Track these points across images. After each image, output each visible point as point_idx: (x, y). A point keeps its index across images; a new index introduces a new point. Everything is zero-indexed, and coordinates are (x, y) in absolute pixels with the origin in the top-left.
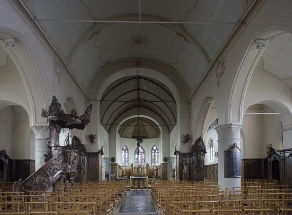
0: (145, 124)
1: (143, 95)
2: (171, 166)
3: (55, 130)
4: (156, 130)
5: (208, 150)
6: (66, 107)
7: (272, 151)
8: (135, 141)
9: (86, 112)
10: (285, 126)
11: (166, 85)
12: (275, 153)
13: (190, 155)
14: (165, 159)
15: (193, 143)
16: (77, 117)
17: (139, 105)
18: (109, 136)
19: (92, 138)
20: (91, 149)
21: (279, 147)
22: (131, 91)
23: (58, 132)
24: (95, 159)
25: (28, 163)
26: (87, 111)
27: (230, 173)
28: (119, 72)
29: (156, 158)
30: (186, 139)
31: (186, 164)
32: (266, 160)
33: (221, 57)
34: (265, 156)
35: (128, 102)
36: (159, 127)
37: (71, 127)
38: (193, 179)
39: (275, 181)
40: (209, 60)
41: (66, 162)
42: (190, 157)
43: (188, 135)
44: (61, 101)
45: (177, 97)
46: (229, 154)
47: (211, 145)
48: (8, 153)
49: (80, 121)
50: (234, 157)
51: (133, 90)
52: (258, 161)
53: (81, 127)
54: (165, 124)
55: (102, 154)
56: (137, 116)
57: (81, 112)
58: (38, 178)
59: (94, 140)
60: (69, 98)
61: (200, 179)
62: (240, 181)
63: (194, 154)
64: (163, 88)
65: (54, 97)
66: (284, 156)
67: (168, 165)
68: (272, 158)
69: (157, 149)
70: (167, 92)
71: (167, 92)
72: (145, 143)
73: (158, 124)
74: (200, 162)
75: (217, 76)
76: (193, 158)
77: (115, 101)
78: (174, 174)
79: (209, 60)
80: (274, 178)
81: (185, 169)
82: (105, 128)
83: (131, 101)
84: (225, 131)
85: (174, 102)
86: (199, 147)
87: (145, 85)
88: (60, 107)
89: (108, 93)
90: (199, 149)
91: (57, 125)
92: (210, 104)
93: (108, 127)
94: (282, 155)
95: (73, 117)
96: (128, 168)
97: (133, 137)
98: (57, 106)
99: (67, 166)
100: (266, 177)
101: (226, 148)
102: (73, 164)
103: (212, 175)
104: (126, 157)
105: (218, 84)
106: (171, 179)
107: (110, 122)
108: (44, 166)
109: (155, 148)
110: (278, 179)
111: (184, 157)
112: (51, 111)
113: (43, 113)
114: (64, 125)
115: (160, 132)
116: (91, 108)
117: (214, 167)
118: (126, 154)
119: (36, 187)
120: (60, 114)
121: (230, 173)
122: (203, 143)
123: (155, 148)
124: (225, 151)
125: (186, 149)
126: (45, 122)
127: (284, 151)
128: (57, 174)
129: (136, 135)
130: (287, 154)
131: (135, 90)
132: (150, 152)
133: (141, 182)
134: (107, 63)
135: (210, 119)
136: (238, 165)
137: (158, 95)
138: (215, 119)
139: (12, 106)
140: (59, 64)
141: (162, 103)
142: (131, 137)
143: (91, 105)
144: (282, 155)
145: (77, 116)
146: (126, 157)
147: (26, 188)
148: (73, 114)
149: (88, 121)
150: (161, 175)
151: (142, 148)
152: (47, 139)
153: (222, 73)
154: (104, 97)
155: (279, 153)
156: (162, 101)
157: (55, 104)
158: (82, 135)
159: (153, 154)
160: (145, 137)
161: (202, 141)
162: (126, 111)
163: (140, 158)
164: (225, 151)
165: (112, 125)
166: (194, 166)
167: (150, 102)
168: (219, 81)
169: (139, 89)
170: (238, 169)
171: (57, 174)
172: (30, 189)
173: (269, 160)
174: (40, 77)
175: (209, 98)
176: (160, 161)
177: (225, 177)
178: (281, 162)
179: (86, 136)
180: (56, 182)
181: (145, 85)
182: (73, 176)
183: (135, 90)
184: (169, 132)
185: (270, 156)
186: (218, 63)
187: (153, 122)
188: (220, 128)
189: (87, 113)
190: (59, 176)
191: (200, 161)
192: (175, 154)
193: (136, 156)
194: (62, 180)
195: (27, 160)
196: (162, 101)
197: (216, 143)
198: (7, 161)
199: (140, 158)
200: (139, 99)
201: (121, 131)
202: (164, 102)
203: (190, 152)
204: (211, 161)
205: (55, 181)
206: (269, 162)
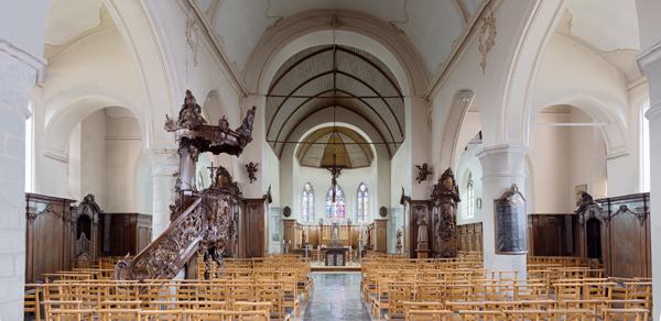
0: (346, 140)
1: (345, 84)
2: (393, 225)
3: (188, 157)
4: (366, 154)
5: (463, 196)
6: (207, 114)
7: (586, 198)
8: (327, 175)
9: (246, 121)
10: (611, 149)
11: (297, 52)
12: (591, 204)
13: (430, 204)
14: (384, 211)
15: (436, 182)
16: (229, 132)
17: (335, 102)
18: (281, 163)
19: (251, 170)
20: (252, 191)
21: (600, 192)
22: (322, 75)
23: (194, 160)
24: (256, 211)
25: (133, 220)
26: (246, 119)
27: (505, 245)
28: (299, 40)
29: (366, 207)
30: (424, 173)
31: (423, 223)
32: (575, 217)
33: (489, 13)
34: (573, 209)
35: (311, 98)
36: (372, 146)
37: (216, 151)
38: (436, 253)
39: (595, 260)
40: (466, 16)
41: (209, 219)
42: (430, 209)
43: (425, 166)
44: (199, 100)
45: (405, 90)
46: (504, 207)
47: (470, 184)
48: (97, 201)
49: (235, 139)
50: (513, 212)
51: (325, 74)
52: (560, 218)
53: (235, 150)
54: (381, 141)
55: (270, 201)
56: (331, 124)
57: (234, 125)
58: (159, 252)
59: (256, 175)
60: (212, 92)
61: (451, 254)
62: (525, 261)
63: (437, 203)
64: (381, 71)
65: (188, 92)
66: (610, 212)
67: (388, 223)
68: (587, 215)
69: (366, 190)
70: (387, 77)
71: (387, 77)
72: (345, 177)
73: (369, 141)
74: (449, 219)
75: (481, 49)
76: (436, 211)
77: (290, 96)
78: (399, 243)
79: (466, 16)
80: (591, 255)
81: (422, 233)
82: (274, 147)
83: (316, 96)
84: (495, 159)
85: (399, 99)
86: (447, 190)
87: (346, 63)
88: (200, 111)
89: (277, 82)
90: (446, 193)
91: (192, 147)
92: (466, 104)
93: (279, 145)
94: (606, 208)
95: (222, 131)
96: (313, 229)
97: (323, 166)
98: (193, 111)
99: (210, 228)
100: (575, 252)
101: (498, 196)
102: (221, 223)
103: (470, 246)
104: (311, 205)
105: (483, 65)
106: (392, 250)
107: (282, 137)
108: (168, 231)
109: (363, 188)
110: (599, 255)
111: (419, 208)
112: (182, 122)
113: (167, 124)
114: (202, 145)
115: (372, 156)
116: (253, 113)
117: (476, 228)
118: (311, 199)
119: (155, 269)
120: (198, 126)
121: (505, 245)
122: (454, 181)
123: (363, 188)
124: (495, 201)
125: (420, 192)
126: (171, 141)
127: (609, 200)
128: (194, 243)
129: (331, 162)
130: (615, 207)
131: (329, 73)
132: (354, 198)
133: (340, 257)
134: (278, 22)
135: (467, 132)
136: (520, 228)
137: (369, 83)
138: (477, 132)
139: (105, 109)
140: (196, 25)
141: (383, 95)
142: (318, 164)
143: (254, 108)
144: (606, 208)
145: (229, 130)
146: (311, 205)
147: (135, 271)
148: (223, 127)
149: (248, 139)
150: (374, 246)
151: (340, 188)
152: (174, 175)
153: (490, 43)
154: (271, 89)
155: (600, 204)
156: (379, 96)
157: (190, 105)
158: (233, 164)
159: (360, 200)
160: (345, 167)
161: (452, 177)
162: (314, 112)
163: (335, 208)
164: (495, 201)
165: (285, 142)
166: (437, 228)
167: (359, 98)
168: (484, 60)
169: (335, 71)
170: (520, 237)
171: (194, 243)
172: (144, 272)
173: (581, 217)
174: (163, 53)
175: (465, 93)
176: (373, 215)
177: (496, 253)
178: (604, 224)
179: (241, 166)
180: (190, 261)
181: (346, 63)
182: (221, 247)
183: (329, 73)
184: (390, 155)
185: (583, 209)
186: (482, 23)
187: (361, 136)
188: (485, 154)
189: (247, 124)
190: (197, 247)
191: (449, 217)
192: (402, 202)
193: (330, 203)
194: (201, 257)
195: (131, 215)
196: (379, 96)
197: (478, 175)
198: (96, 217)
199: (335, 208)
200: (336, 90)
201: (302, 154)
202: (383, 98)
203: (429, 198)
204: (469, 217)
205: (186, 260)
206: (581, 221)
